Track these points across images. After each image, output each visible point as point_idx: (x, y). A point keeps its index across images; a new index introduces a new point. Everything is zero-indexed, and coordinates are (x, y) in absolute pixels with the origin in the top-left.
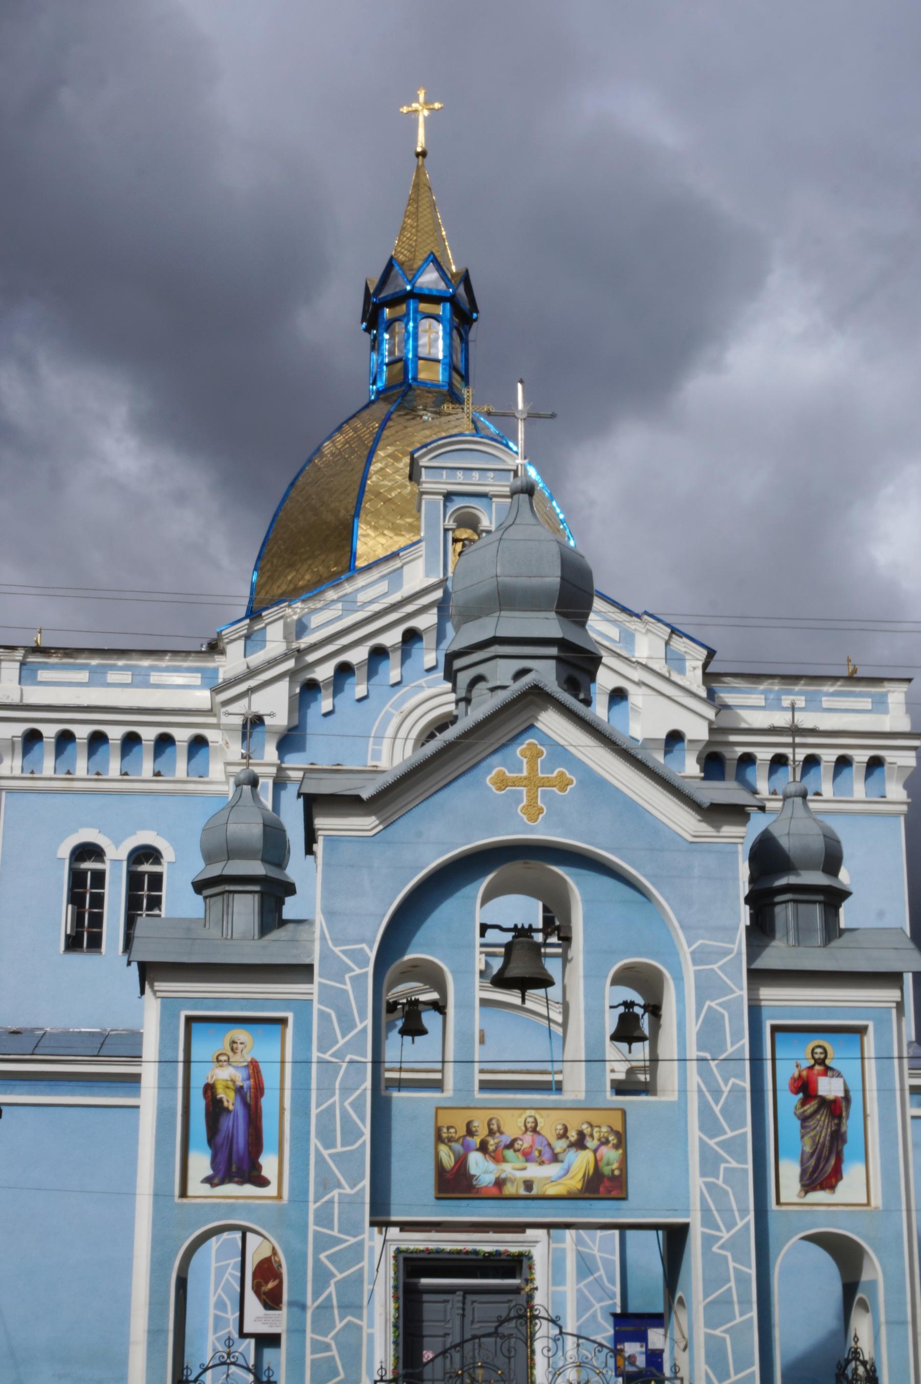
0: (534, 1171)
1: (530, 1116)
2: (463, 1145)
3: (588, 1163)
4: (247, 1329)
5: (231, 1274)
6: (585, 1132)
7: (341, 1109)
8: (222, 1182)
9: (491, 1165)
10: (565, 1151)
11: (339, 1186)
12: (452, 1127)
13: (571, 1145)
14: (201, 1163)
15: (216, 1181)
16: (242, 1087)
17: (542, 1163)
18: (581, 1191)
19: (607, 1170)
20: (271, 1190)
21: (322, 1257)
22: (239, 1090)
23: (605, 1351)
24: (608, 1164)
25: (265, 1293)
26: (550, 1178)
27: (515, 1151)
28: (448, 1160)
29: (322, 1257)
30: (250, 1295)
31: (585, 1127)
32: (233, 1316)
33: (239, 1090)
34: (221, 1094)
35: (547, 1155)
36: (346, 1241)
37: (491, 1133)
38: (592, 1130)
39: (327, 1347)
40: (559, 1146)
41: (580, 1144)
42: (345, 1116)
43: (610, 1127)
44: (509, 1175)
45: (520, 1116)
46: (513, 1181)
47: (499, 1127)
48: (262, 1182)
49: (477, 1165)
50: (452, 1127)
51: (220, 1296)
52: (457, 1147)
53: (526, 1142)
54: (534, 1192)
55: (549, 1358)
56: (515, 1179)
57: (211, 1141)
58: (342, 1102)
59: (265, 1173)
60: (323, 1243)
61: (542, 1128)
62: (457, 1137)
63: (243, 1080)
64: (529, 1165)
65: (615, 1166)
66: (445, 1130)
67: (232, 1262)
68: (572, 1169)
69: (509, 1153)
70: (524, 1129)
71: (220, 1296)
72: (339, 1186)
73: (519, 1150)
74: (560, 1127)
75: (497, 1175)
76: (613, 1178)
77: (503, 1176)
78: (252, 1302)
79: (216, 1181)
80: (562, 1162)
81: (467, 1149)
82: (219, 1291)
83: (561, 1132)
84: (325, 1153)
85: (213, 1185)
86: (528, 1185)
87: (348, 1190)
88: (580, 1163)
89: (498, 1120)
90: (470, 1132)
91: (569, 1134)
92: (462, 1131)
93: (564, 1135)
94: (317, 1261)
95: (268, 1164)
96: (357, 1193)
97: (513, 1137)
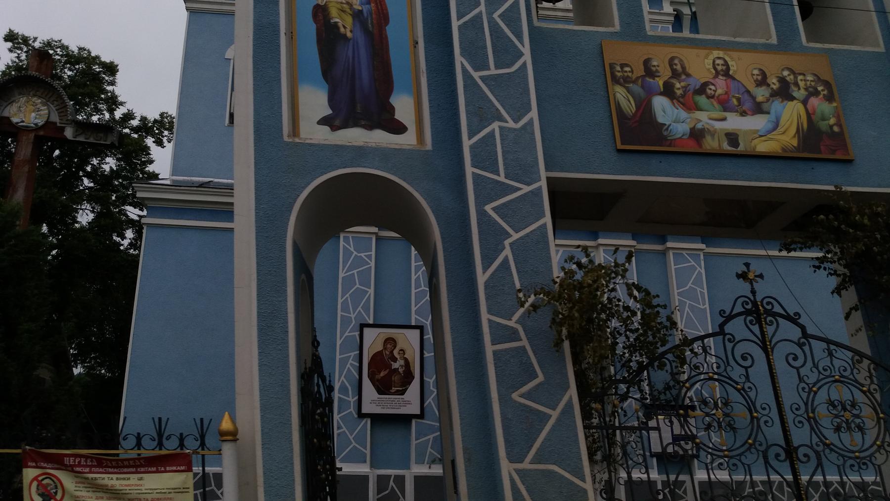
0: (735, 122)
1: (719, 58)
2: (642, 87)
3: (799, 117)
4: (364, 411)
5: (351, 364)
6: (788, 79)
7: (489, 22)
8: (345, 126)
9: (683, 114)
10: (768, 100)
11: (501, 119)
12: (627, 65)
13: (774, 94)
14: (315, 101)
15: (337, 123)
16: (361, 12)
17: (743, 114)
18: (797, 149)
19: (823, 126)
20: (408, 140)
21: (488, 208)
22: (357, 15)
23: (866, 362)
24: (824, 119)
25: (378, 380)
26: (758, 131)
27: (708, 97)
28: (629, 105)
29: (488, 208)
30: (367, 384)
31: (786, 73)
32: (352, 399)
33: (357, 15)
34: (335, 17)
35: (747, 106)
36: (520, 189)
37: (675, 74)
38: (796, 78)
39: (513, 335)
40: (761, 94)
41: (784, 92)
42: (495, 30)
43: (815, 75)
44: (706, 126)
45: (706, 57)
46: (713, 133)
47: (683, 68)
48: (398, 128)
49: (664, 112)
50: (627, 65)
51: (343, 382)
52: (636, 88)
53: (720, 86)
54: (741, 148)
55: (797, 369)
56: (715, 131)
57: (327, 73)
58: (490, 14)
59: (398, 116)
60: (488, 191)
61: (735, 71)
62: (634, 77)
63: (361, 4)
64: (728, 114)
65: (832, 121)
66: (618, 68)
67: (352, 354)
68: (782, 122)
69: (702, 100)
70: (714, 72)
71: (343, 382)
72: (501, 119)
73: (713, 97)
74: (756, 72)
75: (692, 126)
76: (832, 135)
77: (699, 126)
78: (368, 388)
79: (337, 123)
80: (768, 113)
81: (651, 93)
82: (342, 378)
83: (759, 78)
84: (476, 75)
85: (334, 128)
86: (732, 138)
87: (511, 124)
88: (791, 113)
89: (681, 60)
90: (650, 72)
91: (769, 81)
92: (640, 71)
93: (763, 81)
94: (482, 214)
95: (403, 106)
96: (524, 127)
97: (703, 81)
